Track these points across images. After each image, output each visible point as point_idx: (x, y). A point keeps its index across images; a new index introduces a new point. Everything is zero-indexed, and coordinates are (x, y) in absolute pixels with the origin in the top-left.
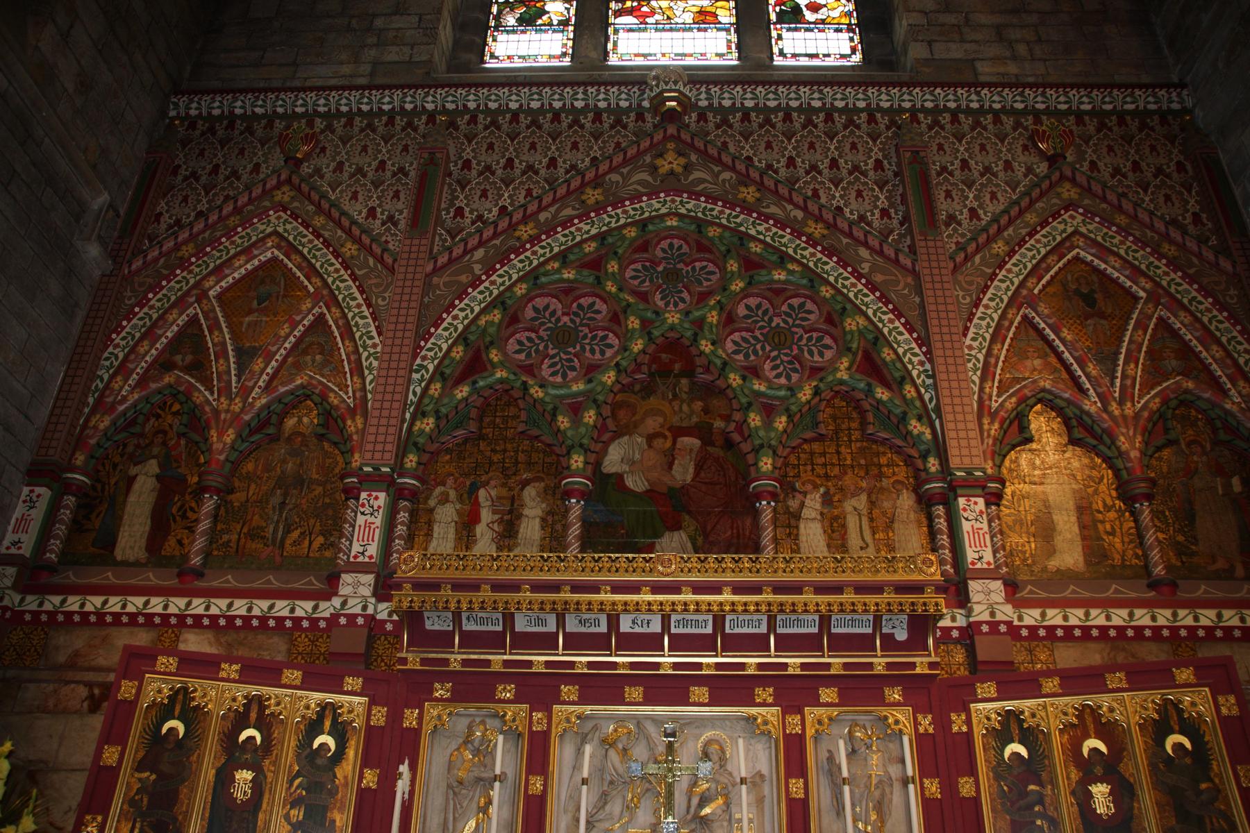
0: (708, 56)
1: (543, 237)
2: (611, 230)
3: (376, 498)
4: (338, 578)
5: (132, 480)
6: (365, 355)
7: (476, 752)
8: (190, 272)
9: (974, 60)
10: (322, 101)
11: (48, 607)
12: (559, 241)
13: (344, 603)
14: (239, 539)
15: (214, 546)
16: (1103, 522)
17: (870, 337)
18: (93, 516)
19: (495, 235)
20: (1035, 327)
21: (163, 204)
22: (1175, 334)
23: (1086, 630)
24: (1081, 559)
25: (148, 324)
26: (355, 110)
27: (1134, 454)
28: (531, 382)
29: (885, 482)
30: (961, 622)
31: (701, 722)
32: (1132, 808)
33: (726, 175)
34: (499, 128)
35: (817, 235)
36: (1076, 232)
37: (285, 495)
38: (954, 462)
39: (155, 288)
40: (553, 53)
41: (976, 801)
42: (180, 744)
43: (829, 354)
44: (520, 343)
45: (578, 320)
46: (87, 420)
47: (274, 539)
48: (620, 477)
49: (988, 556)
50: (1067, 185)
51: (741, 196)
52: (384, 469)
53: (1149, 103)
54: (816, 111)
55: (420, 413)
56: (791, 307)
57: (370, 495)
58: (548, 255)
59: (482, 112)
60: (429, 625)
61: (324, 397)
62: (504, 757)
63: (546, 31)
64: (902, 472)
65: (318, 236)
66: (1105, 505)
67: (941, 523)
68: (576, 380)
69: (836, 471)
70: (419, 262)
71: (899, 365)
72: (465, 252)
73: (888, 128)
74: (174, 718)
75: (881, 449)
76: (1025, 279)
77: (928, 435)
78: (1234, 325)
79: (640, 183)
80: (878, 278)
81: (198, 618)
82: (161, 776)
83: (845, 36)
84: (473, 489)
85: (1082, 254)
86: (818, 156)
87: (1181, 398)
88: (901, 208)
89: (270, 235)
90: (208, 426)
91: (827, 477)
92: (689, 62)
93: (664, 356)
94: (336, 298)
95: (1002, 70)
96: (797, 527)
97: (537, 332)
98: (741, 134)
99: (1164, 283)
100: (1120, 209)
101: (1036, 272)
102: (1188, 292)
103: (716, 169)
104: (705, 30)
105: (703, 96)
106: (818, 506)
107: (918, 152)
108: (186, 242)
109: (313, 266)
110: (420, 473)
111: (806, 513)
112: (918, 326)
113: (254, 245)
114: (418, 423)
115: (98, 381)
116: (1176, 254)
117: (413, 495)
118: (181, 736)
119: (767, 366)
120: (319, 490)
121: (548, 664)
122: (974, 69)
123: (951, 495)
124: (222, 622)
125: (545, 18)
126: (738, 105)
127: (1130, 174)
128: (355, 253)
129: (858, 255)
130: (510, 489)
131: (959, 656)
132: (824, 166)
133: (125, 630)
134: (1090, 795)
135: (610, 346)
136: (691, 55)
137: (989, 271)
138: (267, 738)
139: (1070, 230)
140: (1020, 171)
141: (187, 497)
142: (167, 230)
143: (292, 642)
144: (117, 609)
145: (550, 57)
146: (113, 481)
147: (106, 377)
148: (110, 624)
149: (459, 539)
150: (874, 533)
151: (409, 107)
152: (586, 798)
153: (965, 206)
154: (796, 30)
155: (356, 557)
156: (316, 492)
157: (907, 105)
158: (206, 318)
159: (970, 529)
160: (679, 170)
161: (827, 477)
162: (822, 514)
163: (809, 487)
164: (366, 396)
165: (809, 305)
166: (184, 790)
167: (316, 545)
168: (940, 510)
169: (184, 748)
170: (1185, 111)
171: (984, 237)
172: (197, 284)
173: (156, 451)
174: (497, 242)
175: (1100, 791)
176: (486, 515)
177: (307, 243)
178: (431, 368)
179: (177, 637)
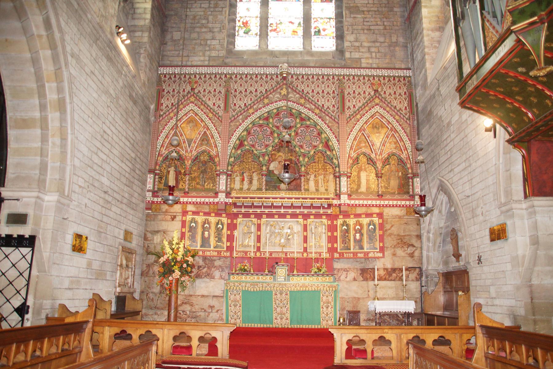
5: (169, 172)
7: (247, 227)
12: (258, 114)
19: (244, 112)
23: (363, 205)
28: (254, 150)
29: (328, 173)
30: (339, 203)
31: (288, 222)
33: (297, 96)
35: (317, 113)
36: (377, 112)
37: (203, 175)
38: (341, 170)
42: (195, 228)
44: (251, 139)
46: (157, 158)
48: (273, 171)
51: (300, 102)
54: (320, 75)
60: (237, 204)
61: (209, 153)
62: (253, 229)
64: (331, 170)
65: (202, 111)
67: (338, 182)
68: (263, 149)
69: (317, 170)
72: (238, 117)
73: (337, 81)
77: (337, 163)
79: (277, 97)
80: (330, 125)
81: (190, 202)
82: (192, 233)
84: (243, 173)
86: (319, 89)
88: (338, 104)
90: (184, 159)
91: (316, 171)
95: (367, 61)
102: (399, 128)
103: (295, 94)
108: (171, 112)
109: (202, 119)
111: (311, 179)
112: (337, 137)
113: (187, 113)
117: (231, 175)
120: (210, 174)
121: (260, 211)
122: (361, 61)
124: (195, 203)
127: (393, 95)
131: (338, 209)
135: (270, 140)
137: (355, 123)
138: (210, 226)
139: (376, 111)
140: (367, 93)
143: (210, 207)
147: (159, 148)
151: (220, 72)
152: (268, 236)
158: (179, 133)
165: (315, 130)
166: (197, 236)
167: (211, 186)
168: (338, 179)
169: (195, 228)
170: (410, 77)
171: (356, 113)
173: (173, 165)
174: (244, 114)
175: (358, 235)
176: (246, 179)
178: (232, 146)
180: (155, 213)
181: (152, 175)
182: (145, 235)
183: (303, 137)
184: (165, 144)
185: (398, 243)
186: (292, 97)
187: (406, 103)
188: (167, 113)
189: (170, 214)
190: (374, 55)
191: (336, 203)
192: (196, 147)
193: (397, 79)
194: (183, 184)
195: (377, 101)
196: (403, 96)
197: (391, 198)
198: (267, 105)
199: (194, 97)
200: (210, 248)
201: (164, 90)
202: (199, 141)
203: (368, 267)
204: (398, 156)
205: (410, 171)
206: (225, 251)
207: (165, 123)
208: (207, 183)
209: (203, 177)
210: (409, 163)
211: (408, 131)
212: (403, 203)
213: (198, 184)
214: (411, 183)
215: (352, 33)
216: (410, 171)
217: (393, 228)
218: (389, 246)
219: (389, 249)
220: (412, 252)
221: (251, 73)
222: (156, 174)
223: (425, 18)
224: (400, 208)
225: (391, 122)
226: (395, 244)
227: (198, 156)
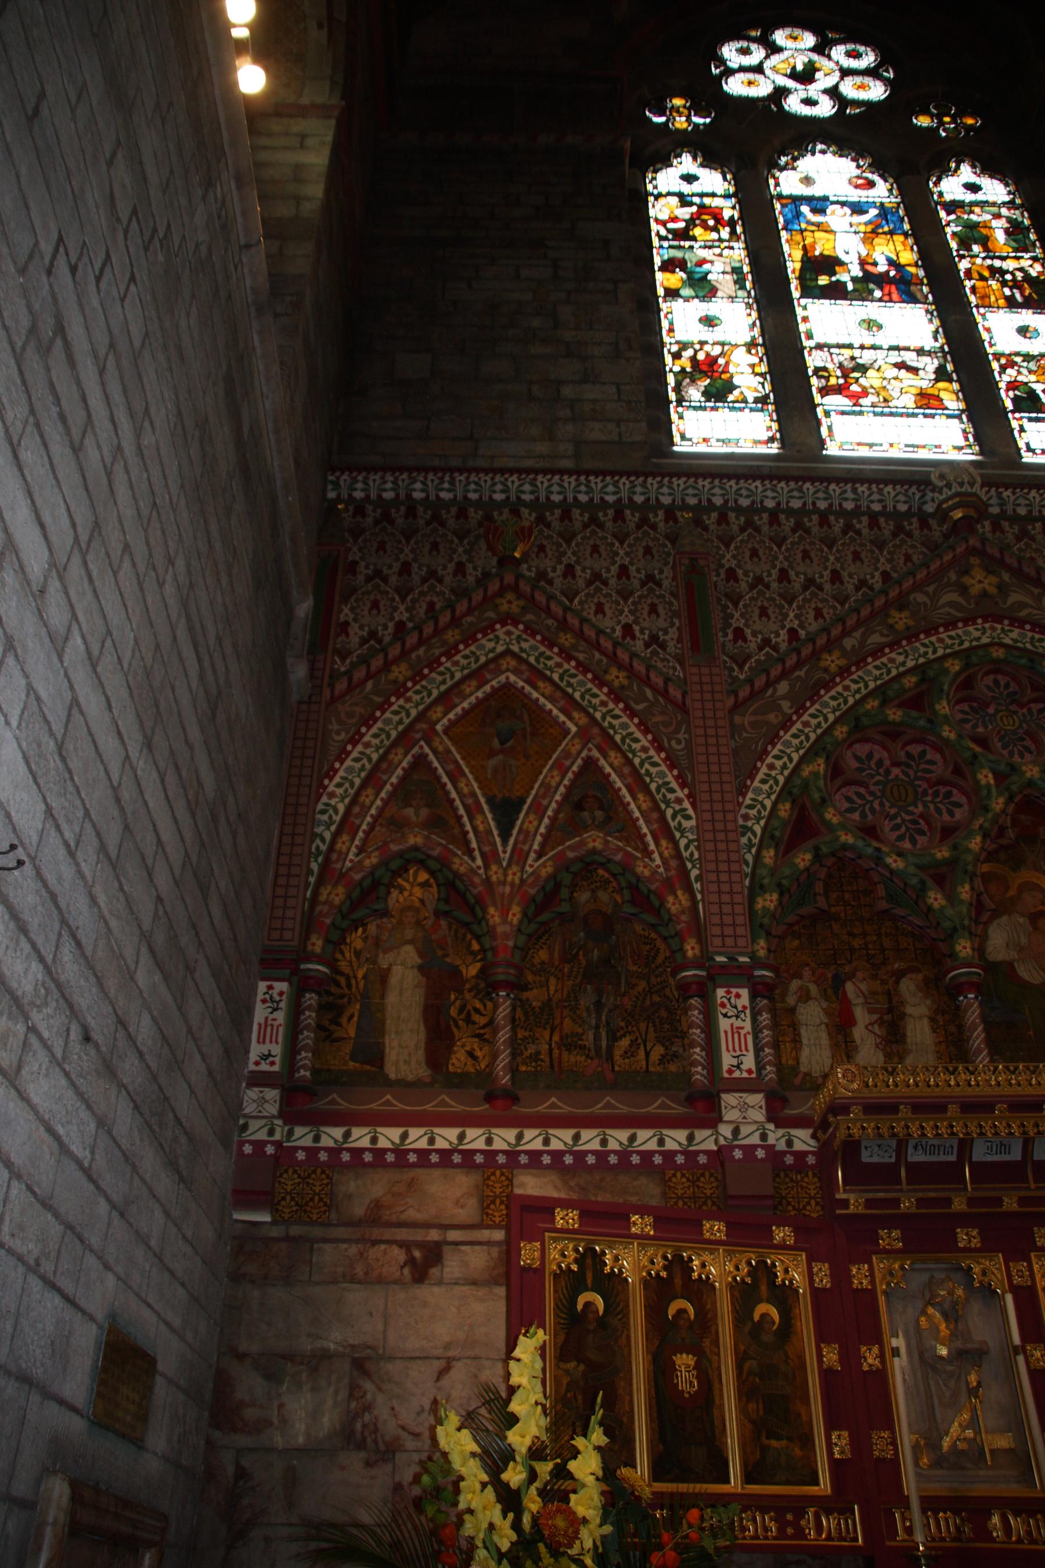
0: (944, 449)
1: (853, 669)
2: (930, 662)
3: (738, 996)
5: (384, 977)
6: (669, 812)
8: (409, 700)
10: (527, 487)
11: (326, 1142)
12: (871, 675)
13: (736, 1131)
14: (551, 1050)
15: (519, 1059)
18: (344, 1020)
21: (346, 610)
25: (368, 766)
26: (570, 499)
28: (885, 849)
36: (508, 652)
39: (369, 721)
40: (757, 438)
42: (602, 1323)
43: (959, 814)
44: (849, 799)
45: (911, 772)
46: (316, 893)
47: (598, 1048)
48: (1010, 965)
49: (749, 1062)
50: (510, 596)
52: (742, 959)
53: (523, 492)
55: (757, 888)
57: (728, 992)
58: (864, 692)
59: (732, 509)
63: (742, 410)
74: (587, 1290)
79: (951, 604)
84: (838, 983)
85: (513, 678)
90: (480, 900)
92: (923, 455)
93: (1023, 817)
94: (611, 738)
97: (867, 787)
98: (615, 536)
101: (446, 700)
104: (932, 416)
108: (396, 661)
109: (570, 697)
114: (760, 900)
115: (318, 841)
118: (601, 1312)
119: (887, 825)
123: (710, 985)
124: (568, 1160)
125: (736, 392)
128: (625, 682)
130: (883, 982)
133: (437, 1173)
134: (673, 1368)
136: (924, 447)
139: (500, 649)
141: (468, 996)
142: (361, 645)
144: (423, 1144)
145: (756, 442)
146: (360, 974)
147: (328, 836)
148: (414, 1165)
149: (834, 1046)
151: (639, 499)
153: (619, 622)
155: (730, 1072)
156: (640, 988)
160: (992, 590)
164: (684, 866)
172: (421, 716)
173: (409, 933)
174: (801, 673)
176: (860, 1014)
177: (457, 667)
179: (510, 1180)
180: (295, 1230)
181: (282, 986)
182: (222, 1382)
184: (362, 815)
186: (1025, 605)
188: (377, 663)
189: (403, 1234)
192: (546, 837)
194: (474, 1044)
198: (909, 639)
199: (520, 595)
200: (727, 1481)
201: (352, 567)
202: (560, 804)
204: (433, 865)
206: (825, 1505)
207: (359, 710)
208: (625, 1043)
209: (599, 1005)
213: (570, 1044)
221: (796, 504)
222: (302, 984)
227: (558, 886)
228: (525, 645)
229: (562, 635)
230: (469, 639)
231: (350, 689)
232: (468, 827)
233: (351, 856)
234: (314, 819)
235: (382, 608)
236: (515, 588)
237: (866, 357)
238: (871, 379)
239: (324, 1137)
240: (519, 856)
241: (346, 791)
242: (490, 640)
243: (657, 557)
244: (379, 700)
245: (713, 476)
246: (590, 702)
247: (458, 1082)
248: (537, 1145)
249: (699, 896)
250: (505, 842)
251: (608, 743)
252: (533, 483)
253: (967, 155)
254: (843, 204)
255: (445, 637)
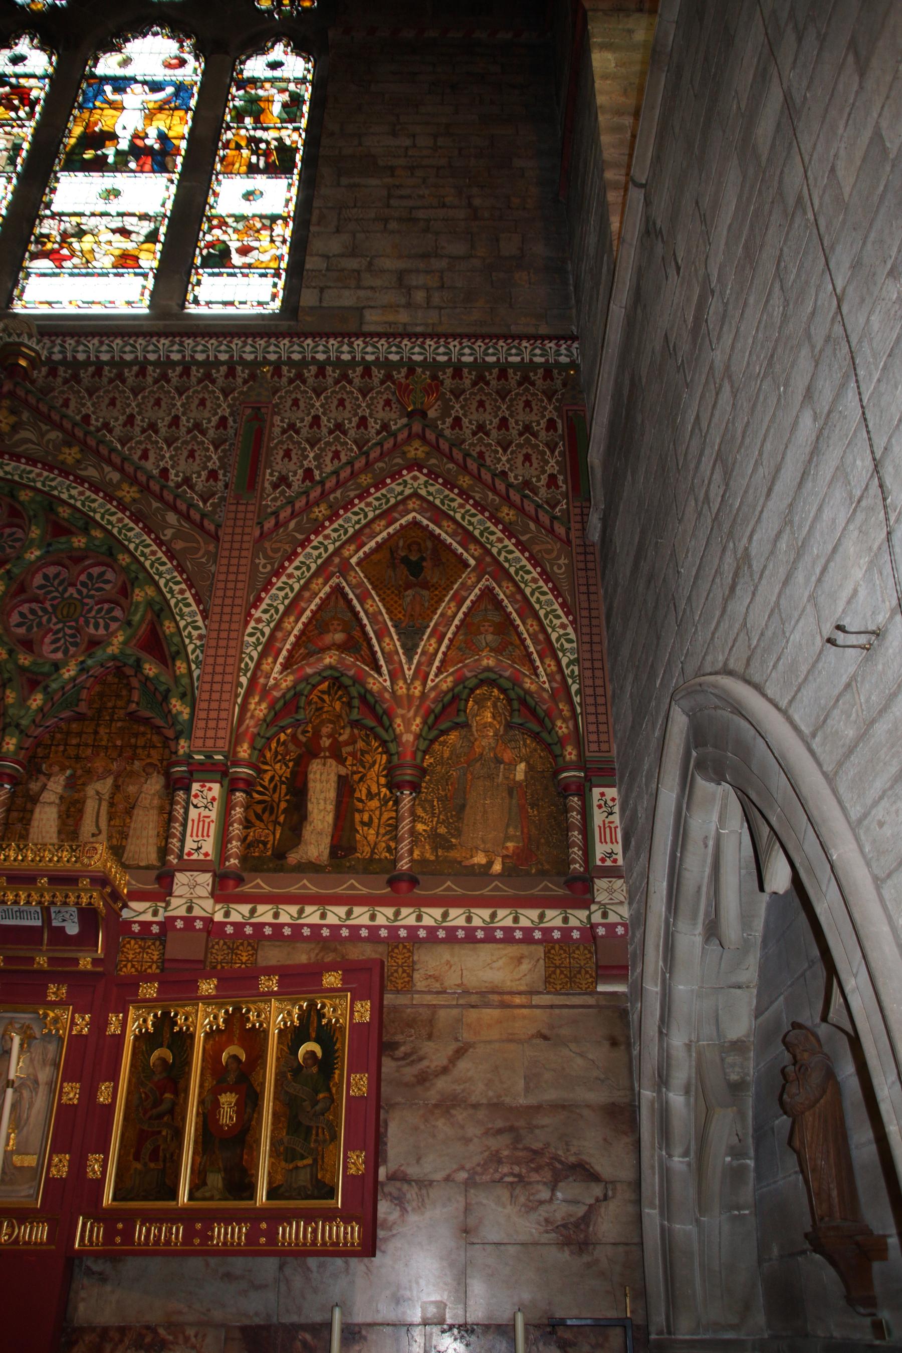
0: (117, 304)
3: (210, 789)
4: (172, 877)
9: (364, 308)
10: (345, 348)
16: (361, 811)
17: (157, 608)
20: (345, 596)
22: (499, 605)
23: (297, 928)
24: (327, 852)
27: (408, 738)
32: (250, 1120)
33: (54, 435)
34: (304, 382)
35: (128, 499)
36: (415, 495)
39: (291, 556)
41: (110, 1108)
50: (417, 443)
51: (61, 457)
52: (217, 757)
53: (535, 355)
56: (90, 576)
59: (285, 364)
66: (369, 793)
69: (89, 752)
70: (247, 530)
71: (176, 639)
75: (142, 729)
76: (342, 546)
78: (556, 598)
80: (179, 545)
83: (270, 280)
85: (419, 517)
87: (481, 676)
89: (409, 497)
90: (389, 714)
91: (78, 758)
95: (391, 318)
96: (32, 812)
99: (495, 551)
100: (465, 468)
101: (357, 539)
102: (517, 560)
103: (44, 428)
104: (122, 275)
105: (57, 349)
106: (59, 790)
107: (259, 409)
109: (470, 535)
110: (254, 760)
116: (513, 518)
123: (587, 784)
126: (93, 358)
129: (164, 520)
132: (351, 425)
139: (408, 492)
140: (374, 426)
150: (110, 819)
153: (302, 466)
154: (220, 274)
157: (223, 357)
159: (196, 818)
161: (78, 758)
162: (61, 798)
163: (56, 768)
175: (228, 1100)
177: (459, 508)
183: (48, 605)
185: (496, 1159)
187: (552, 462)
190: (419, 296)
191: (148, 917)
193: (514, 377)
195: (417, 450)
196: (543, 434)
197: (460, 891)
203: (295, 1319)
204: (507, 685)
205: (570, 753)
210: (567, 713)
211: (559, 570)
212: (529, 917)
214: (575, 817)
215: (338, 231)
216: (570, 753)
217: (463, 1065)
218: (439, 1176)
219: (434, 1193)
220: (581, 1211)
223: (605, 77)
224: (512, 950)
225: (477, 533)
226: (478, 1159)
228: (431, 489)
229: (461, 477)
230: (379, 484)
231: (277, 525)
232: (377, 648)
233: (274, 675)
234: (243, 642)
235: (197, 458)
236: (423, 438)
237: (89, 223)
238: (87, 242)
239: (233, 913)
240: (421, 675)
241: (272, 616)
242: (399, 484)
243: (535, 411)
244: (300, 537)
245: (101, 335)
246: (488, 538)
247: (370, 867)
248: (509, 922)
249: (579, 710)
250: (410, 660)
251: (501, 573)
252: (350, 344)
253: (285, 35)
254: (144, 83)
255: (359, 481)
